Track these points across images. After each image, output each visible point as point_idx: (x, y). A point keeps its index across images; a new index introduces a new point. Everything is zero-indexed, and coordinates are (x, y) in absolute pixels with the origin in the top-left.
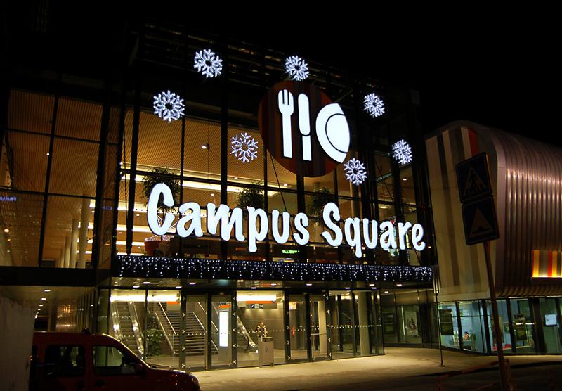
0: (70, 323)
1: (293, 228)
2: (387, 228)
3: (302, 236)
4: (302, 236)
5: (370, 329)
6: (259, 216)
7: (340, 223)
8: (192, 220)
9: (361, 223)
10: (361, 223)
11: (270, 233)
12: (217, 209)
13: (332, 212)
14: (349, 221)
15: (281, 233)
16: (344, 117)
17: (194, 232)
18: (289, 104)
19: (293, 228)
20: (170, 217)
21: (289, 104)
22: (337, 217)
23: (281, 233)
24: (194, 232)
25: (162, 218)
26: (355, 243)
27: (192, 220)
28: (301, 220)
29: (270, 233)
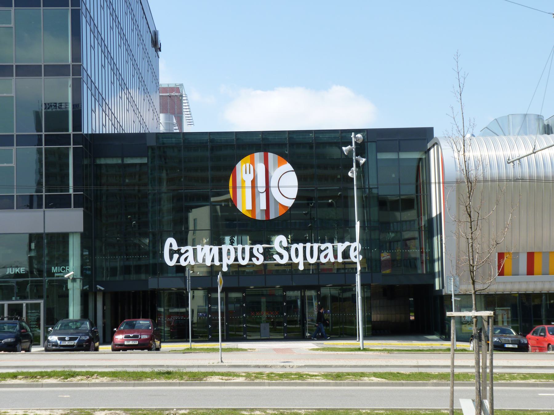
0: (538, 395)
1: (252, 255)
2: (187, 251)
3: (258, 259)
4: (258, 259)
5: (54, 280)
6: (229, 250)
7: (288, 249)
8: (328, 253)
9: (305, 248)
10: (305, 248)
11: (236, 259)
12: (202, 249)
13: (281, 242)
14: (294, 246)
15: (312, 256)
16: (294, 172)
17: (329, 259)
18: (250, 173)
19: (252, 255)
20: (176, 256)
21: (250, 173)
22: (285, 244)
23: (312, 256)
24: (329, 259)
25: (171, 258)
26: (299, 260)
27: (328, 253)
28: (258, 249)
29: (236, 259)
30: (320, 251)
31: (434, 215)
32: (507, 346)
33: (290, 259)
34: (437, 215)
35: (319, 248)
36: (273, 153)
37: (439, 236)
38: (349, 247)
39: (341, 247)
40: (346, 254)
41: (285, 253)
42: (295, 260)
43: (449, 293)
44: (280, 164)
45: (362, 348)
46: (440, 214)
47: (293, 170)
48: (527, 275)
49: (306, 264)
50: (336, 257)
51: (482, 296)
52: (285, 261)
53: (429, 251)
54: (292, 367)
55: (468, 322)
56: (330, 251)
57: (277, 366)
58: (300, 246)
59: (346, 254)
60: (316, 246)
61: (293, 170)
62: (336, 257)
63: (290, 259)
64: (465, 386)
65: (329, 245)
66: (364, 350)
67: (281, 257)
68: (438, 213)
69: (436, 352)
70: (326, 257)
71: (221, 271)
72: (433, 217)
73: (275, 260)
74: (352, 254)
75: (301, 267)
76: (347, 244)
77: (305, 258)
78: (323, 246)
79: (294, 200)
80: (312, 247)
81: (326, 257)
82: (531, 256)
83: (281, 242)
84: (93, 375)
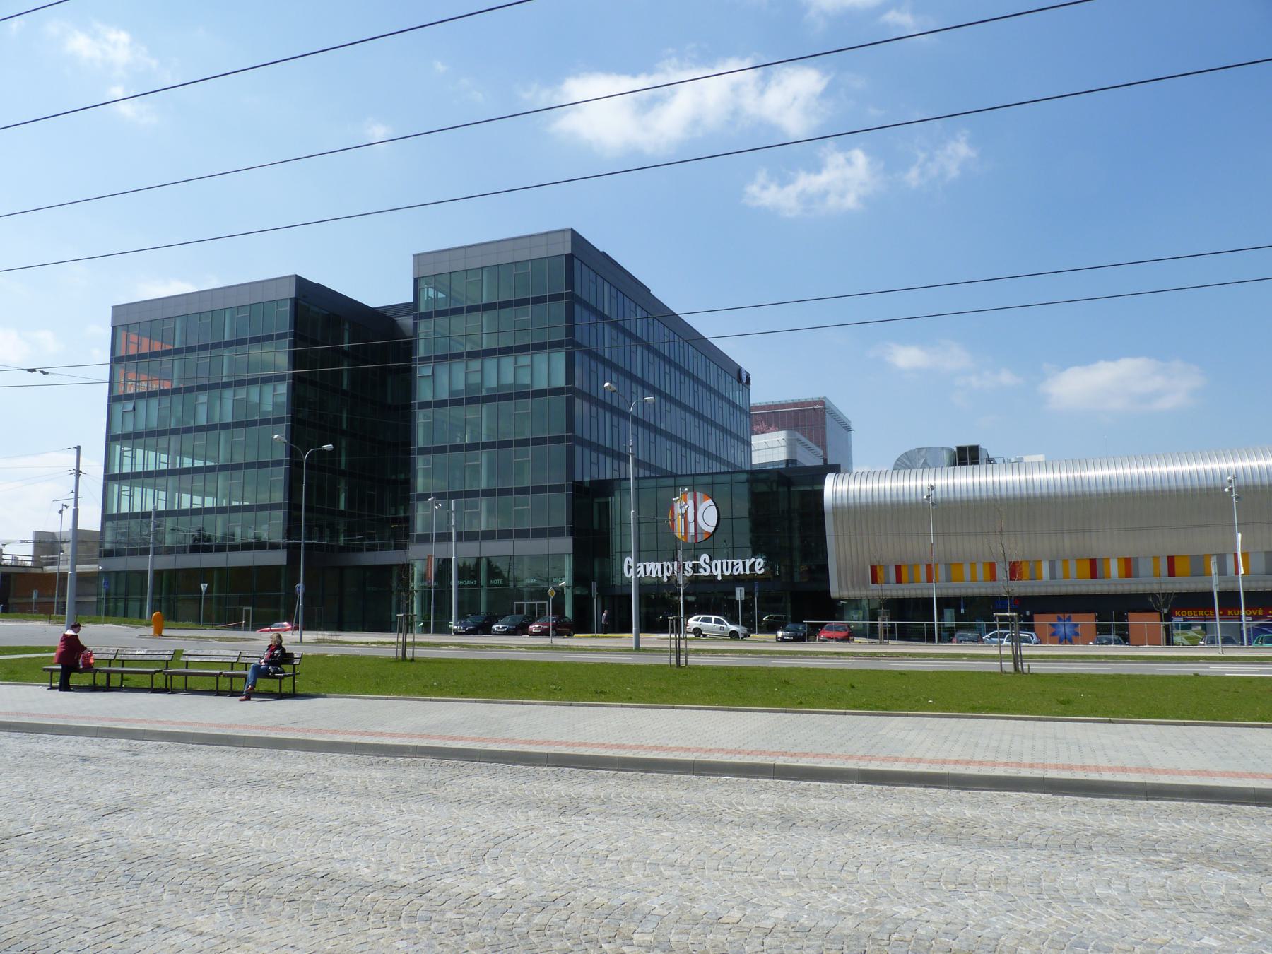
9: (722, 563)
10: (722, 563)
15: (727, 570)
22: (708, 561)
23: (727, 570)
30: (733, 566)
33: (711, 572)
36: (805, 467)
39: (749, 562)
40: (752, 567)
42: (715, 573)
49: (722, 575)
50: (744, 570)
56: (741, 565)
59: (752, 567)
62: (744, 570)
63: (711, 572)
65: (740, 561)
67: (705, 570)
70: (737, 570)
74: (757, 568)
76: (753, 560)
78: (735, 562)
80: (727, 563)
81: (737, 570)
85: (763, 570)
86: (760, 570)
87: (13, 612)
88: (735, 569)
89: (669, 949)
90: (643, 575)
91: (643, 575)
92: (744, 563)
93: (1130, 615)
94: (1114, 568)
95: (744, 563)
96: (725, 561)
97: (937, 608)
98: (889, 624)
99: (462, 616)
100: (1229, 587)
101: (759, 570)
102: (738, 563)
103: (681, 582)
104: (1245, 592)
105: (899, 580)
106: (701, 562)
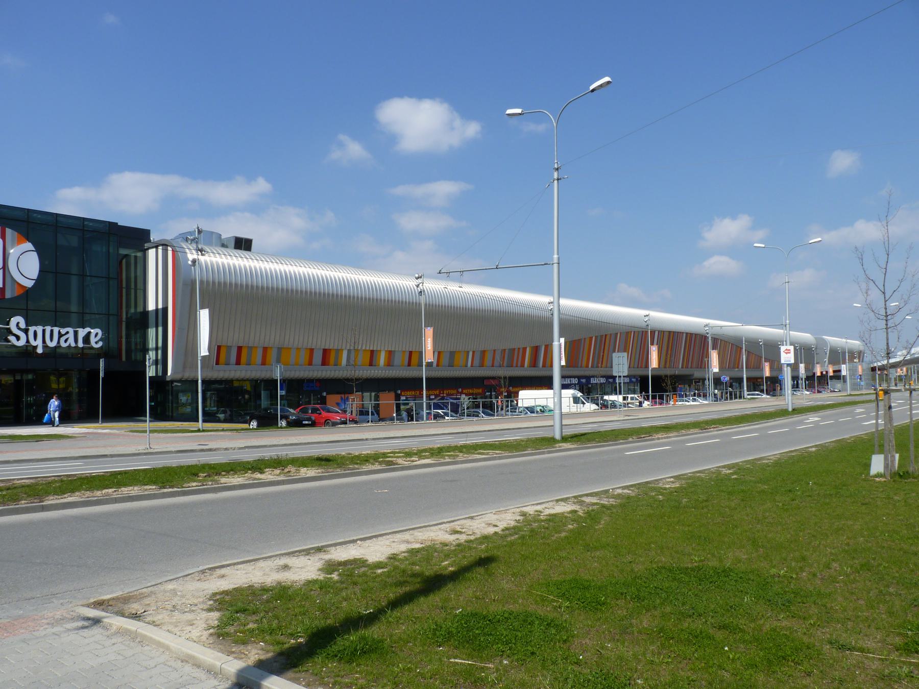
7: (26, 331)
9: (44, 331)
10: (44, 331)
13: (18, 323)
14: (32, 329)
15: (51, 340)
22: (23, 325)
23: (51, 340)
30: (60, 335)
31: (151, 306)
32: (304, 422)
33: (28, 341)
34: (157, 310)
35: (59, 332)
36: (12, 229)
37: (160, 329)
38: (90, 333)
39: (82, 332)
40: (87, 339)
41: (22, 335)
42: (33, 343)
43: (276, 378)
44: (19, 243)
45: (201, 430)
46: (165, 310)
47: (34, 250)
48: (236, 365)
49: (45, 346)
50: (76, 340)
51: (254, 381)
52: (22, 343)
53: (140, 341)
54: (234, 449)
55: (184, 404)
56: (71, 336)
57: (221, 448)
58: (39, 329)
59: (87, 339)
60: (56, 330)
61: (34, 250)
62: (76, 340)
63: (28, 341)
64: (44, 461)
65: (71, 330)
66: (203, 431)
67: (18, 338)
68: (160, 306)
69: (730, 427)
70: (66, 341)
71: (777, 361)
72: (148, 311)
73: (9, 341)
74: (93, 340)
75: (40, 350)
76: (88, 329)
77: (44, 341)
78: (63, 331)
79: (34, 281)
80: (52, 331)
81: (66, 341)
82: (240, 349)
83: (18, 323)
84: (196, 475)
85: (100, 344)
86: (96, 343)
87: (553, 374)
88: (63, 339)
89: (797, 688)
90: (73, 345)
91: (73, 345)
92: (76, 333)
93: (268, 392)
94: (382, 359)
95: (76, 333)
96: (48, 329)
97: (651, 387)
98: (428, 397)
99: (600, 391)
100: (188, 375)
101: (96, 342)
102: (67, 333)
103: (847, 363)
104: (426, 379)
105: (238, 362)
106: (13, 326)
